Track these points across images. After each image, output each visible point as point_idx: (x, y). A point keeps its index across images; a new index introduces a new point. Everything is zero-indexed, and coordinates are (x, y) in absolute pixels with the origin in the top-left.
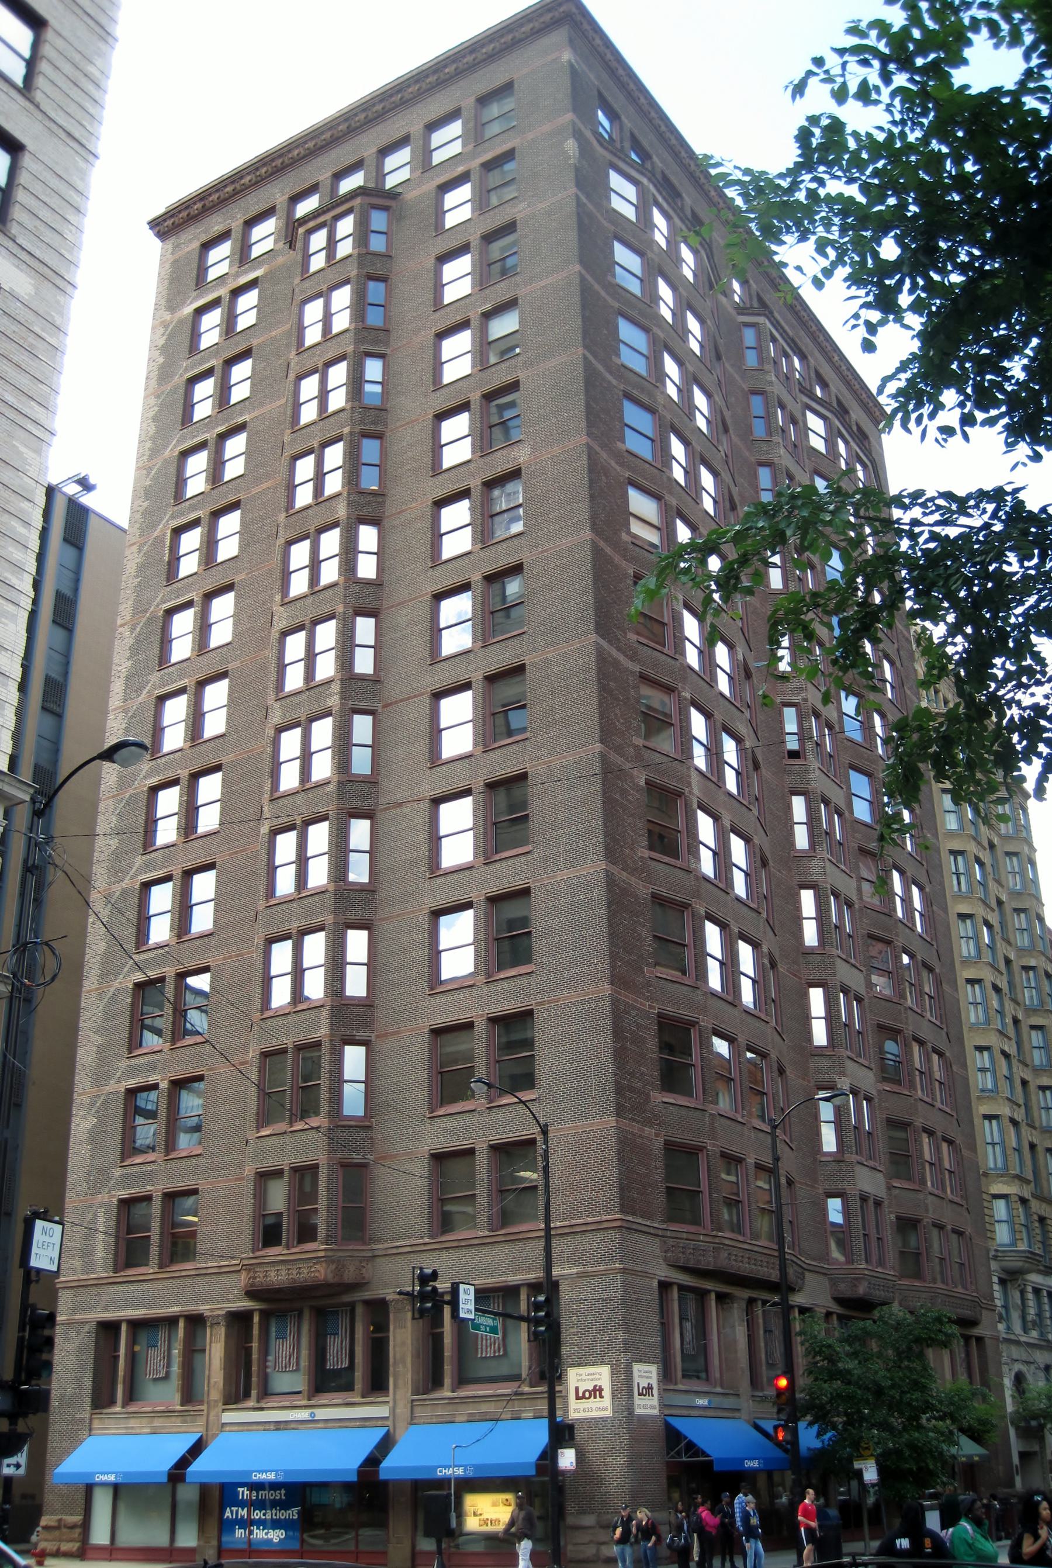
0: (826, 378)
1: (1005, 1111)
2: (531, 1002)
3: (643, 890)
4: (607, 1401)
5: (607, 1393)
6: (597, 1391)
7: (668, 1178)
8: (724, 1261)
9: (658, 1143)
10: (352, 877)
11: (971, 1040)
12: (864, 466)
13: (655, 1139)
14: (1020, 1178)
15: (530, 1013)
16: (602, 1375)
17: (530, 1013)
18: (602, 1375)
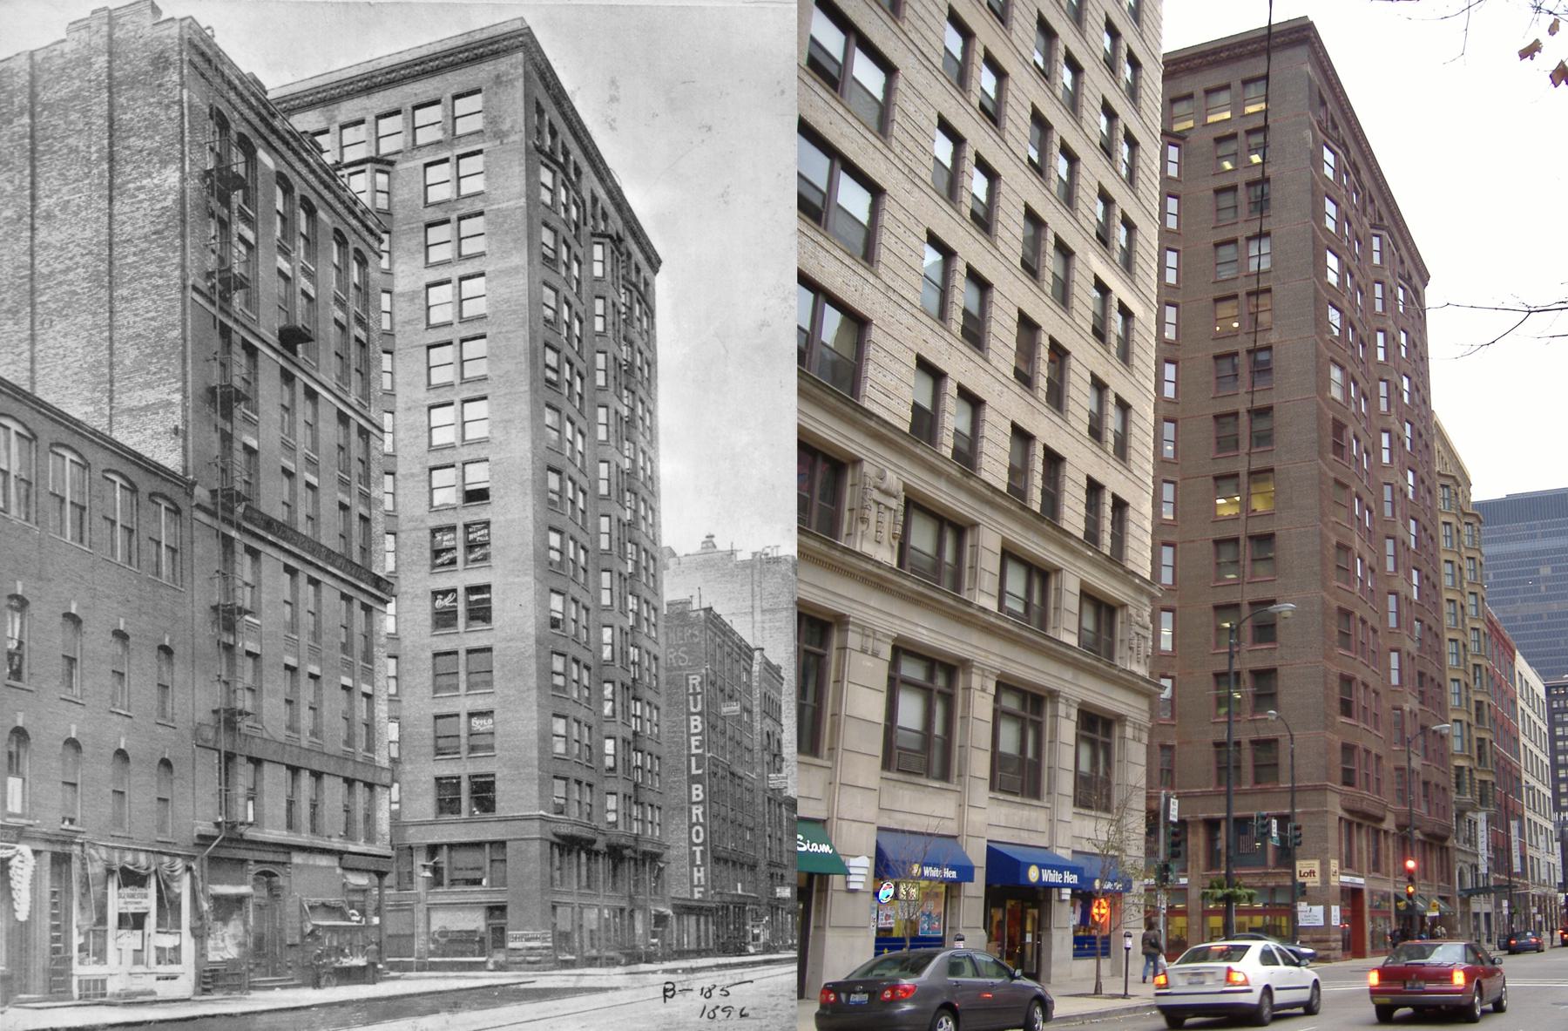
0: (1133, 442)
1: (1464, 717)
2: (1276, 664)
3: (1335, 604)
4: (1317, 878)
5: (1317, 874)
6: (1312, 873)
7: (1343, 762)
8: (1365, 807)
9: (1338, 745)
10: (1165, 516)
11: (1450, 675)
12: (578, 208)
13: (1337, 741)
14: (1470, 757)
15: (1275, 670)
16: (1315, 865)
17: (1275, 670)
18: (1315, 865)
